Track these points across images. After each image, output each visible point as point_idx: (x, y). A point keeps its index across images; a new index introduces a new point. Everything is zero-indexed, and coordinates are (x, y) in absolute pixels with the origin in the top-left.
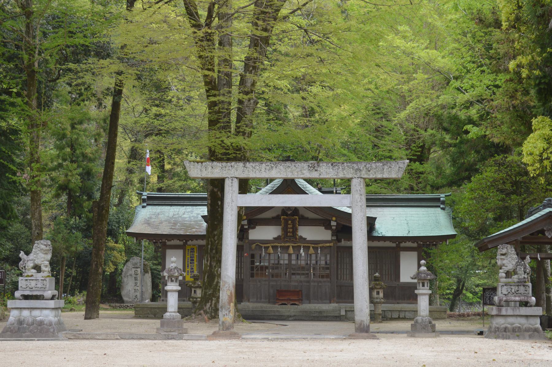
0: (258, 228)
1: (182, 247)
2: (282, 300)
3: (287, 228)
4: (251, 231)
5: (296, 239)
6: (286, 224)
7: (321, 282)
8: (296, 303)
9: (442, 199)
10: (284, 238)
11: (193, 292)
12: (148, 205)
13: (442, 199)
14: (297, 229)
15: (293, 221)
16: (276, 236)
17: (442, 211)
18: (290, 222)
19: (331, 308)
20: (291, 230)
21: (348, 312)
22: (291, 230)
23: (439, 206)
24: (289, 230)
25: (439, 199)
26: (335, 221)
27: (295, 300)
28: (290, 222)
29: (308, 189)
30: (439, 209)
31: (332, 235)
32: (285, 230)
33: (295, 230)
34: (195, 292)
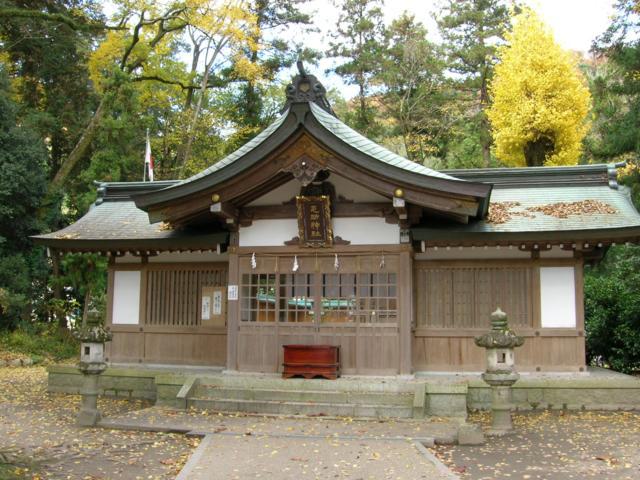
0: (256, 223)
1: (143, 265)
2: (297, 367)
3: (309, 221)
4: (242, 230)
5: (328, 242)
6: (307, 214)
7: (378, 329)
8: (324, 373)
9: (610, 171)
10: (305, 241)
11: (83, 351)
12: (105, 201)
13: (610, 171)
14: (327, 223)
15: (320, 205)
16: (290, 239)
17: (613, 191)
18: (313, 208)
19: (395, 388)
20: (317, 225)
21: (432, 397)
22: (317, 225)
23: (607, 184)
24: (313, 224)
25: (605, 171)
26: (402, 197)
27: (324, 368)
28: (313, 208)
29: (340, 131)
30: (607, 189)
31: (402, 234)
32: (306, 227)
33: (324, 227)
34: (87, 351)
